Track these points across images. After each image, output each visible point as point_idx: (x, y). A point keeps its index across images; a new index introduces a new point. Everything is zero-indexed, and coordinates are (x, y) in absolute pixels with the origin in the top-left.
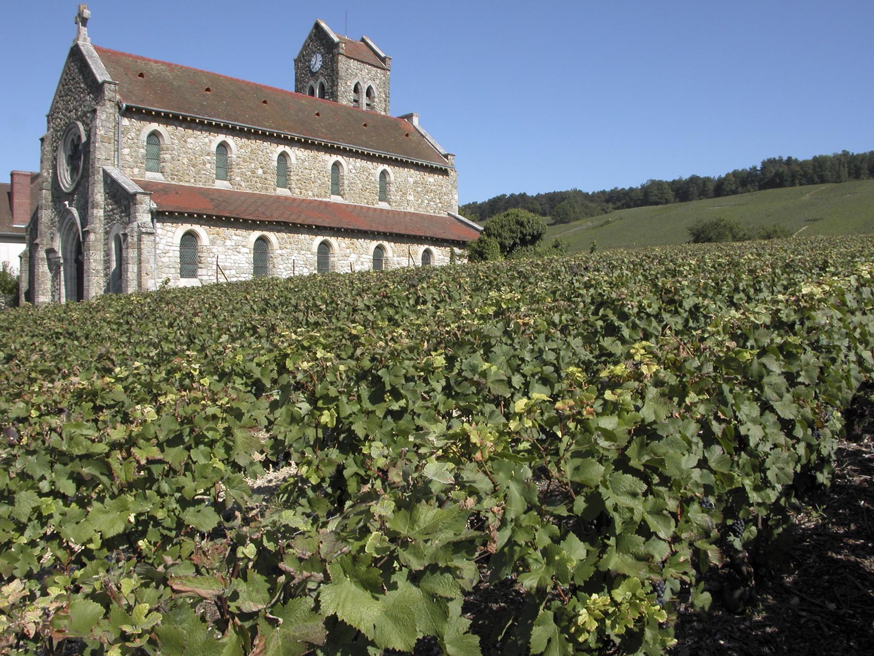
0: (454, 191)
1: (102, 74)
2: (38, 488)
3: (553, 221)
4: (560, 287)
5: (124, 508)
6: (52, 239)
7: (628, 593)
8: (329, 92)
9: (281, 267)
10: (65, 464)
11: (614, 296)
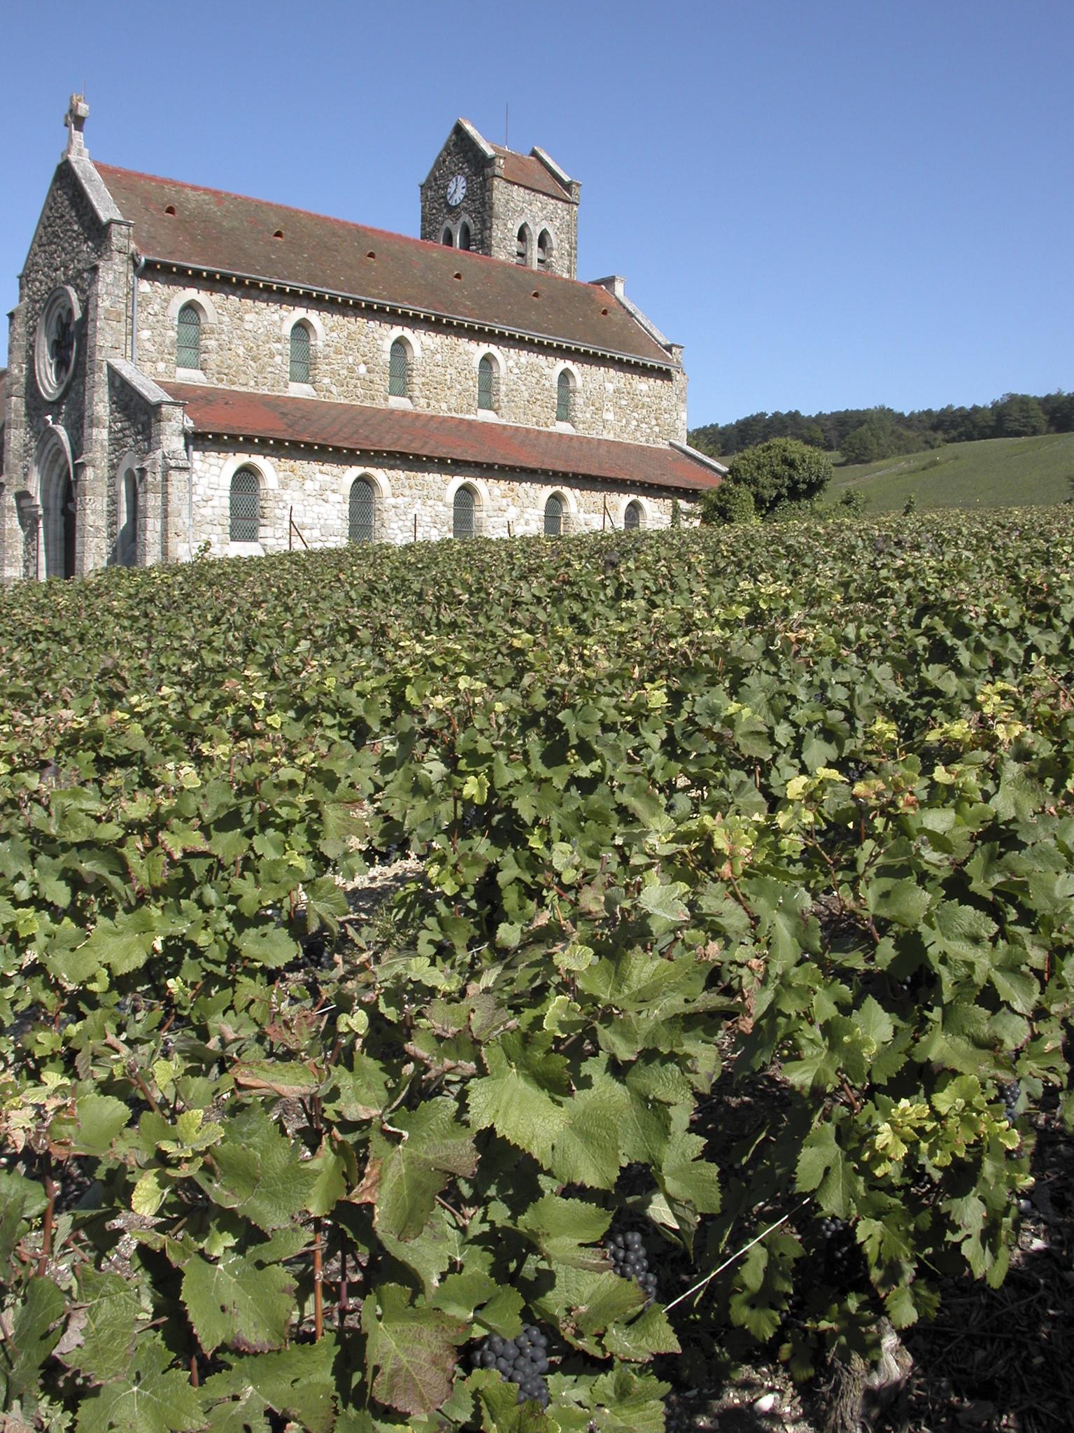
0: (681, 406)
1: (107, 209)
2: (12, 893)
3: (844, 459)
4: (856, 576)
5: (146, 928)
6: (26, 476)
7: (959, 1100)
8: (477, 240)
9: (394, 525)
10: (55, 857)
11: (946, 595)
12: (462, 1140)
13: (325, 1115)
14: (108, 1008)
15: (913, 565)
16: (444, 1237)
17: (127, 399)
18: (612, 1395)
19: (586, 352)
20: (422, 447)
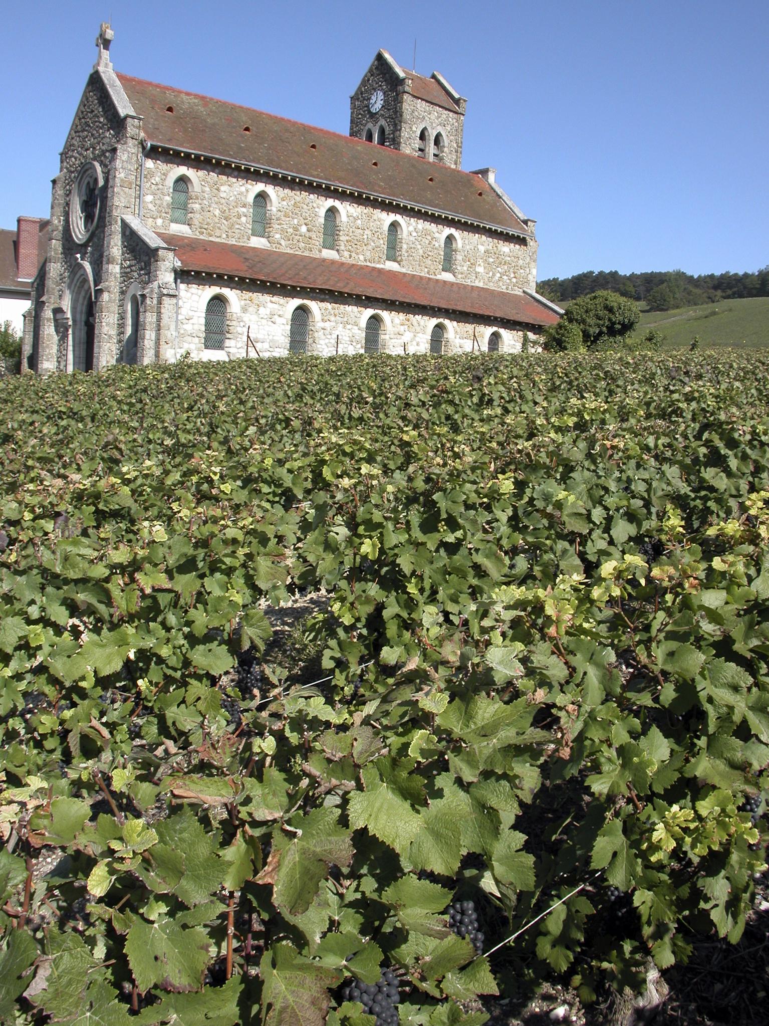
0: (533, 264)
1: (125, 107)
2: (26, 613)
3: (648, 308)
4: (655, 398)
5: (123, 643)
6: (60, 296)
8: (391, 138)
9: (321, 342)
11: (723, 417)
12: (343, 837)
13: (240, 816)
14: (93, 699)
15: (698, 391)
16: (327, 904)
17: (134, 244)
18: (446, 1021)
19: (466, 223)
20: (345, 287)
